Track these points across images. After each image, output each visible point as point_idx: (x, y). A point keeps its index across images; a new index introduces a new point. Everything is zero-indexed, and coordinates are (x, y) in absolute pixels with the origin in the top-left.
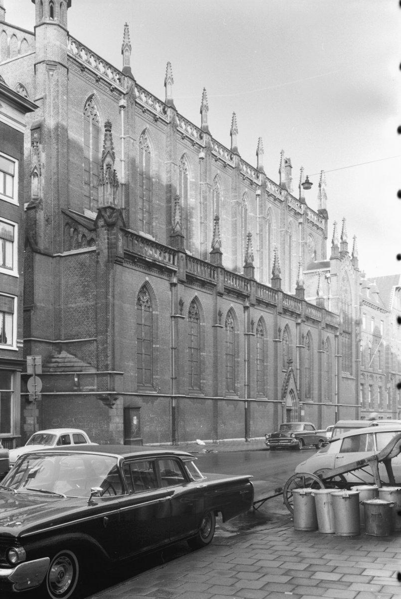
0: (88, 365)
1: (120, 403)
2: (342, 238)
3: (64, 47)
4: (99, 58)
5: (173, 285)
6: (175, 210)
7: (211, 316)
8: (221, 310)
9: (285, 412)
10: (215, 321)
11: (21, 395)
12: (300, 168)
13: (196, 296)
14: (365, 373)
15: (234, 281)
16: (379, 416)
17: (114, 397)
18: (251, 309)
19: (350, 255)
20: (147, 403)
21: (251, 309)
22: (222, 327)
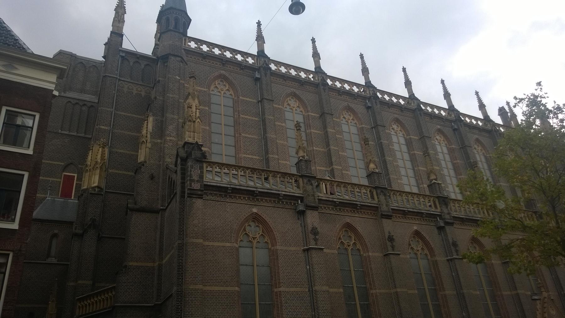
18: (448, 228)
21: (448, 228)
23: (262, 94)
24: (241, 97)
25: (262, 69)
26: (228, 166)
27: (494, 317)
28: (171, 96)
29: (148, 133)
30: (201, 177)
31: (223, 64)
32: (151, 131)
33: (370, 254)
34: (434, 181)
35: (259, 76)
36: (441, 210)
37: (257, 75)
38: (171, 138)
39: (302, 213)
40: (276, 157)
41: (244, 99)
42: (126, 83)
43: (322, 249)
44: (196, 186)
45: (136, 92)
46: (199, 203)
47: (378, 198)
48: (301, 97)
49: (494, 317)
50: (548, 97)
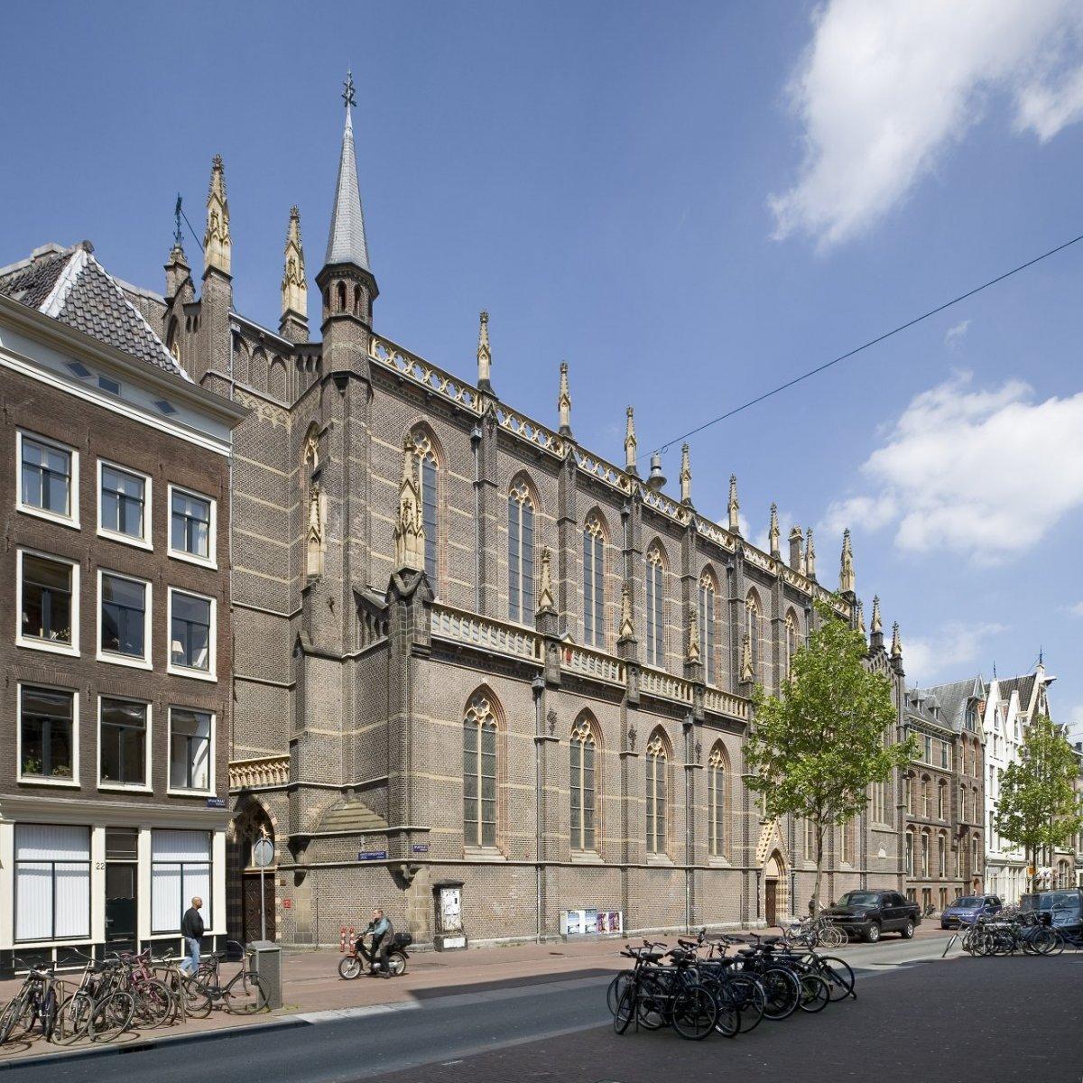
0: (380, 818)
1: (422, 878)
2: (873, 627)
3: (362, 350)
4: (533, 425)
5: (538, 692)
6: (743, 656)
7: (618, 737)
8: (635, 729)
9: (763, 887)
10: (624, 745)
11: (107, 864)
12: (770, 506)
13: (720, 739)
14: (931, 827)
15: (685, 690)
16: (956, 887)
17: (413, 867)
18: (695, 729)
19: (888, 650)
20: (656, 878)
21: (695, 729)
22: (701, 768)
23: (482, 473)
24: (450, 472)
25: (485, 420)
26: (468, 617)
27: (1081, 951)
28: (355, 460)
29: (322, 526)
30: (428, 627)
31: (427, 401)
32: (325, 521)
33: (606, 751)
34: (694, 660)
35: (480, 436)
36: (694, 702)
37: (478, 433)
38: (357, 541)
39: (538, 692)
40: (495, 588)
41: (455, 475)
42: (245, 394)
43: (557, 741)
44: (423, 641)
45: (263, 416)
46: (423, 665)
47: (628, 678)
48: (535, 481)
49: (1081, 951)
50: (876, 601)
